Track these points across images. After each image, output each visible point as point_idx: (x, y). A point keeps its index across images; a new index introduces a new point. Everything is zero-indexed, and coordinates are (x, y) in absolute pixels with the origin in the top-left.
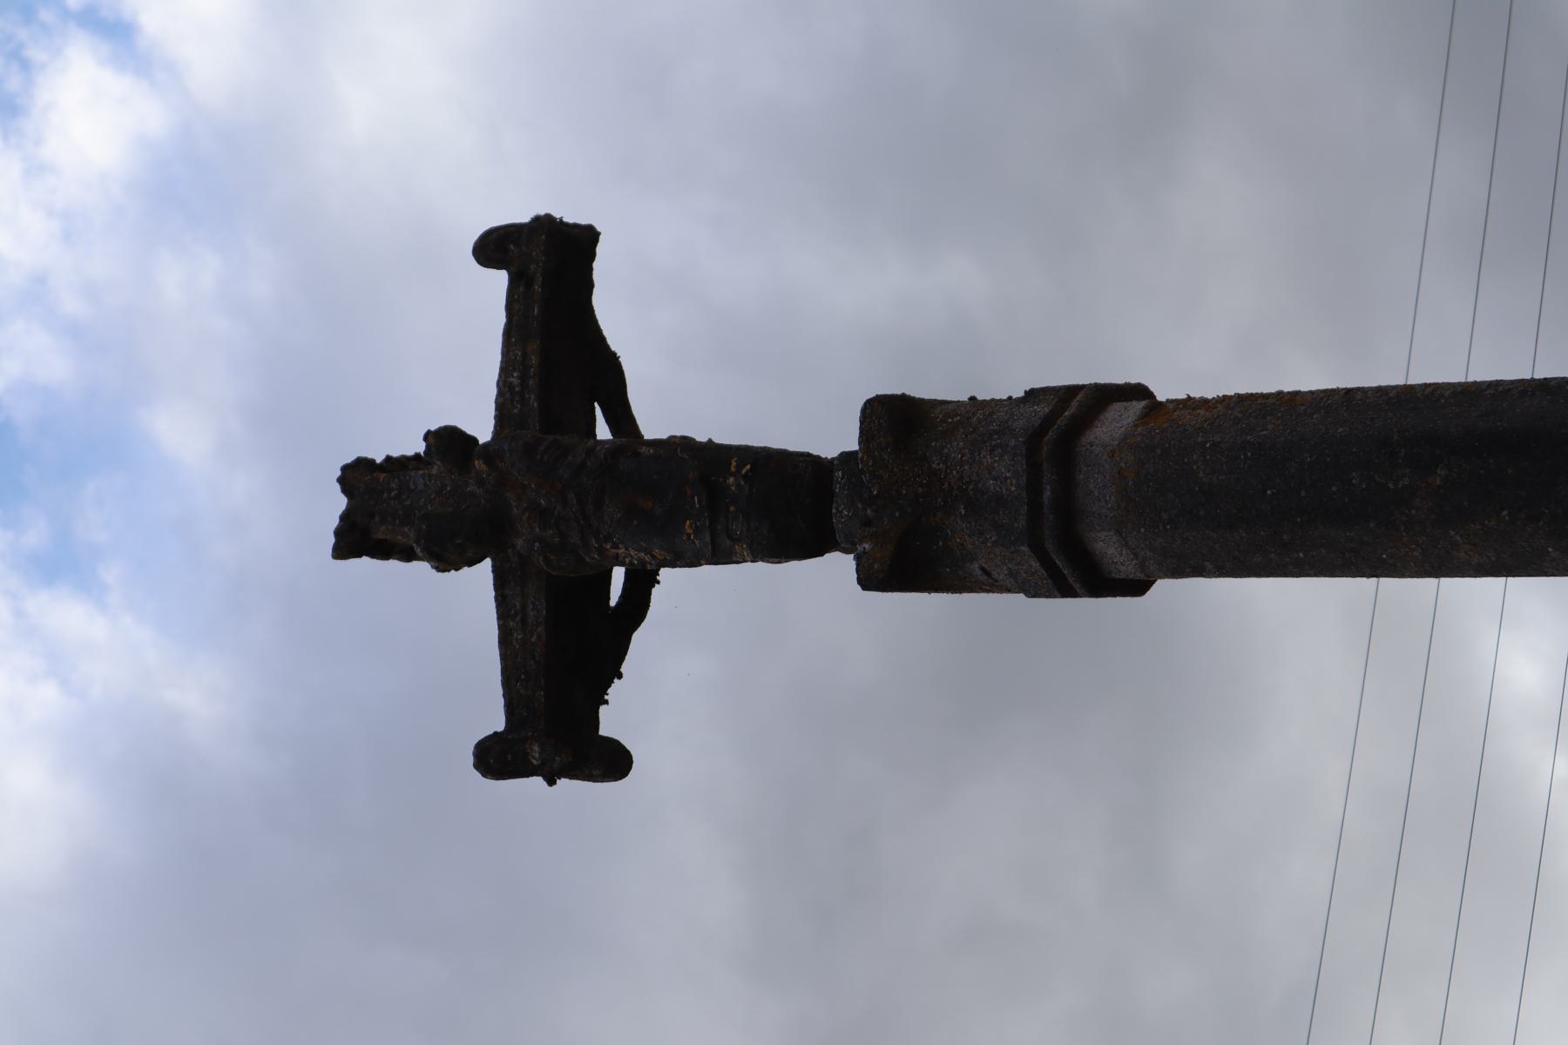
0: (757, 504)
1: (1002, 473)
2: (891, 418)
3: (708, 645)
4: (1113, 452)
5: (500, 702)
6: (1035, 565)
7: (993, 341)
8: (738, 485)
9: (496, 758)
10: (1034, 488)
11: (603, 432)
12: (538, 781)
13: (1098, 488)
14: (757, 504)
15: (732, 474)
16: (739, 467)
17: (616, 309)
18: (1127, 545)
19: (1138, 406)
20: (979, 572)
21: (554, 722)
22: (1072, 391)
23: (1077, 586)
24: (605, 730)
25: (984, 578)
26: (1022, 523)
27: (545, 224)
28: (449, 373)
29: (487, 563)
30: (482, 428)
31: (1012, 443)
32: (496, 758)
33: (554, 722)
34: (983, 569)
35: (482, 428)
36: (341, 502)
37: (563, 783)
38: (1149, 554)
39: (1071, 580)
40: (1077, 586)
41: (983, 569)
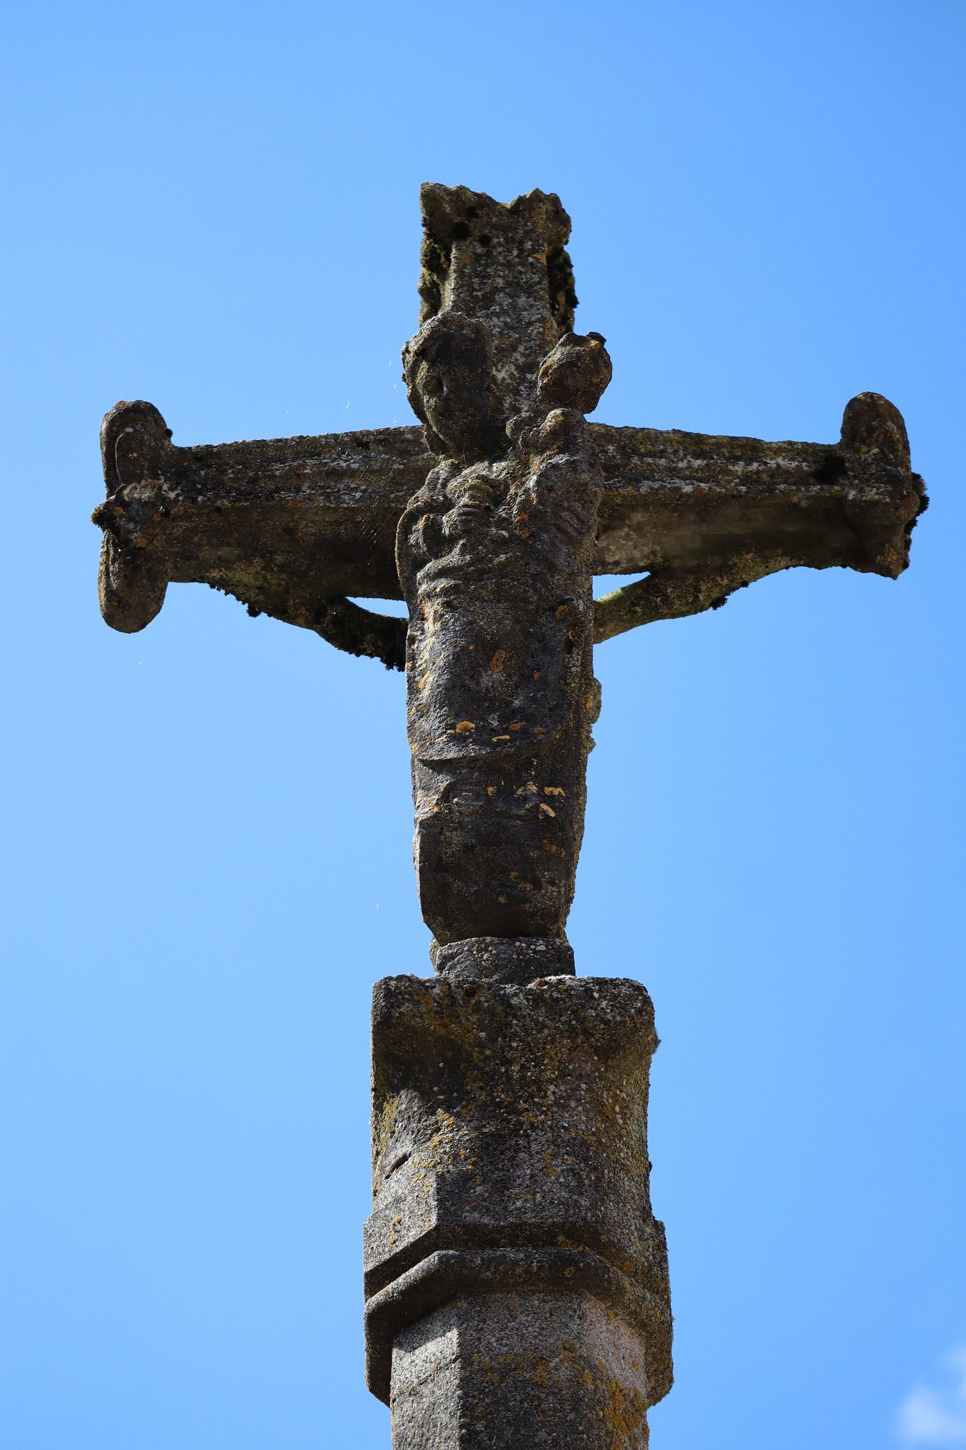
0: (500, 848)
1: (541, 1186)
2: (618, 1026)
3: (305, 760)
4: (571, 1350)
5: (216, 439)
6: (411, 1236)
7: (706, 1152)
8: (525, 799)
9: (134, 436)
10: (519, 1235)
11: (606, 587)
12: (99, 495)
13: (522, 1325)
14: (500, 848)
15: (541, 788)
16: (551, 800)
17: (791, 601)
18: (439, 1369)
19: (638, 1383)
20: (400, 1153)
21: (182, 515)
22: (662, 1291)
23: (379, 1297)
24: (176, 592)
25: (392, 1159)
26: (471, 1217)
27: (911, 496)
28: (692, 352)
29: (410, 420)
30: (613, 410)
31: (584, 1202)
32: (134, 436)
33: (182, 515)
34: (405, 1158)
35: (613, 410)
36: (506, 197)
37: (98, 536)
38: (426, 1401)
39: (390, 1287)
40: (379, 1297)
41: (405, 1158)
